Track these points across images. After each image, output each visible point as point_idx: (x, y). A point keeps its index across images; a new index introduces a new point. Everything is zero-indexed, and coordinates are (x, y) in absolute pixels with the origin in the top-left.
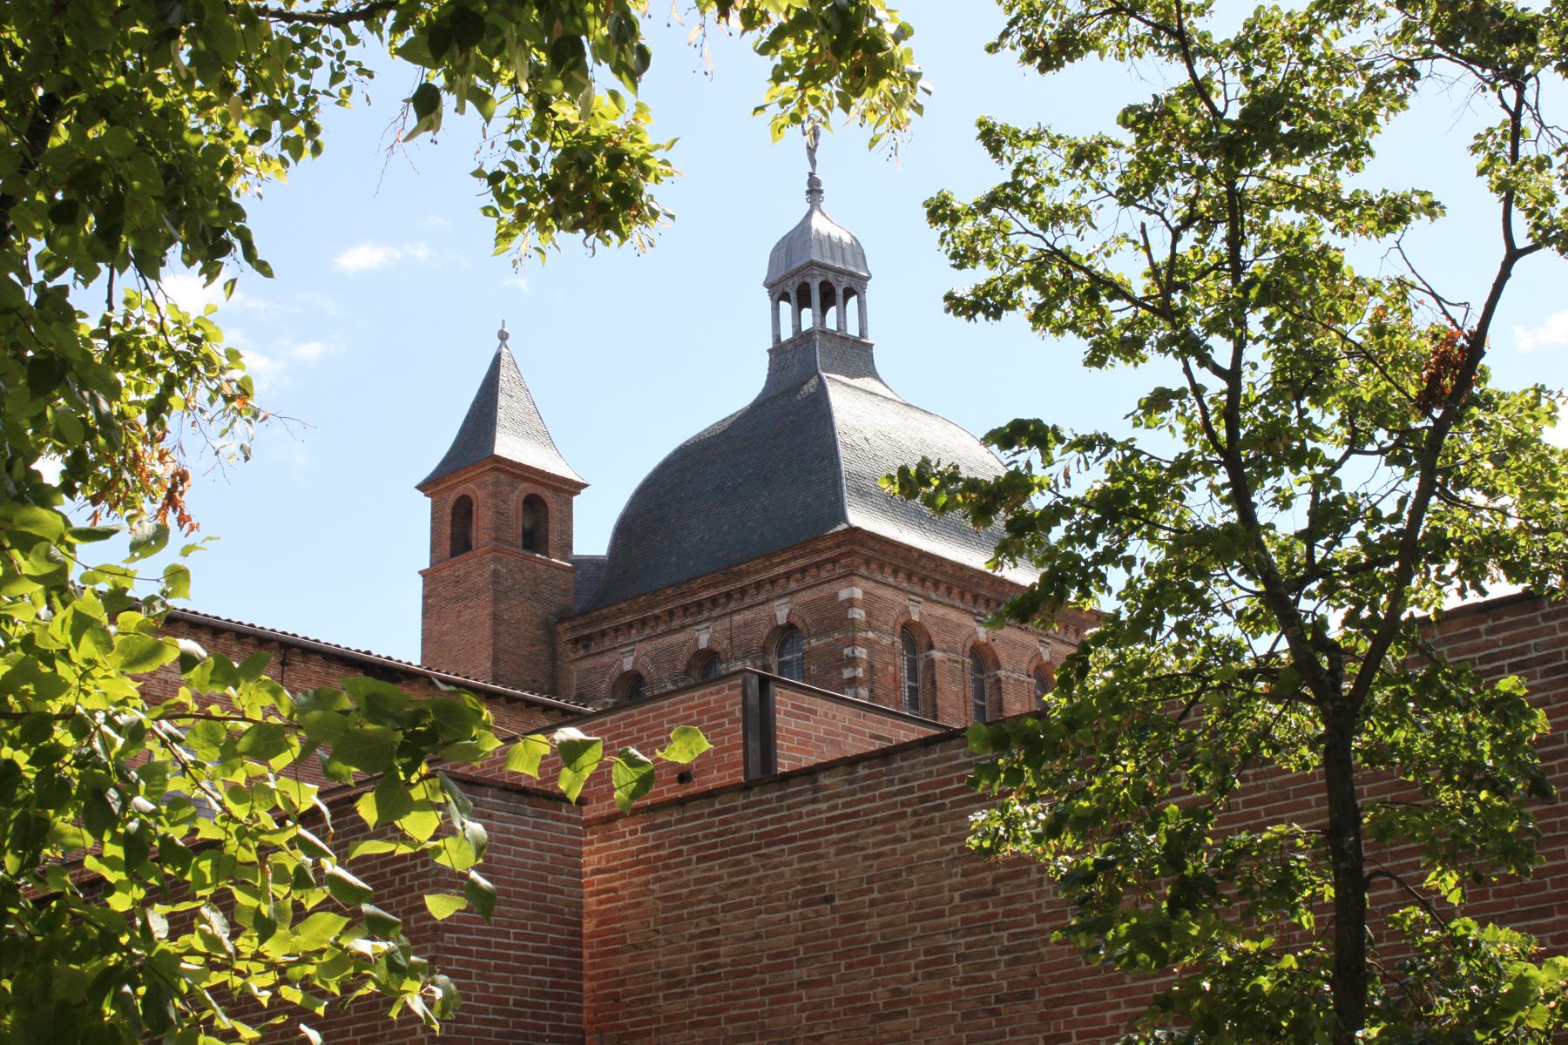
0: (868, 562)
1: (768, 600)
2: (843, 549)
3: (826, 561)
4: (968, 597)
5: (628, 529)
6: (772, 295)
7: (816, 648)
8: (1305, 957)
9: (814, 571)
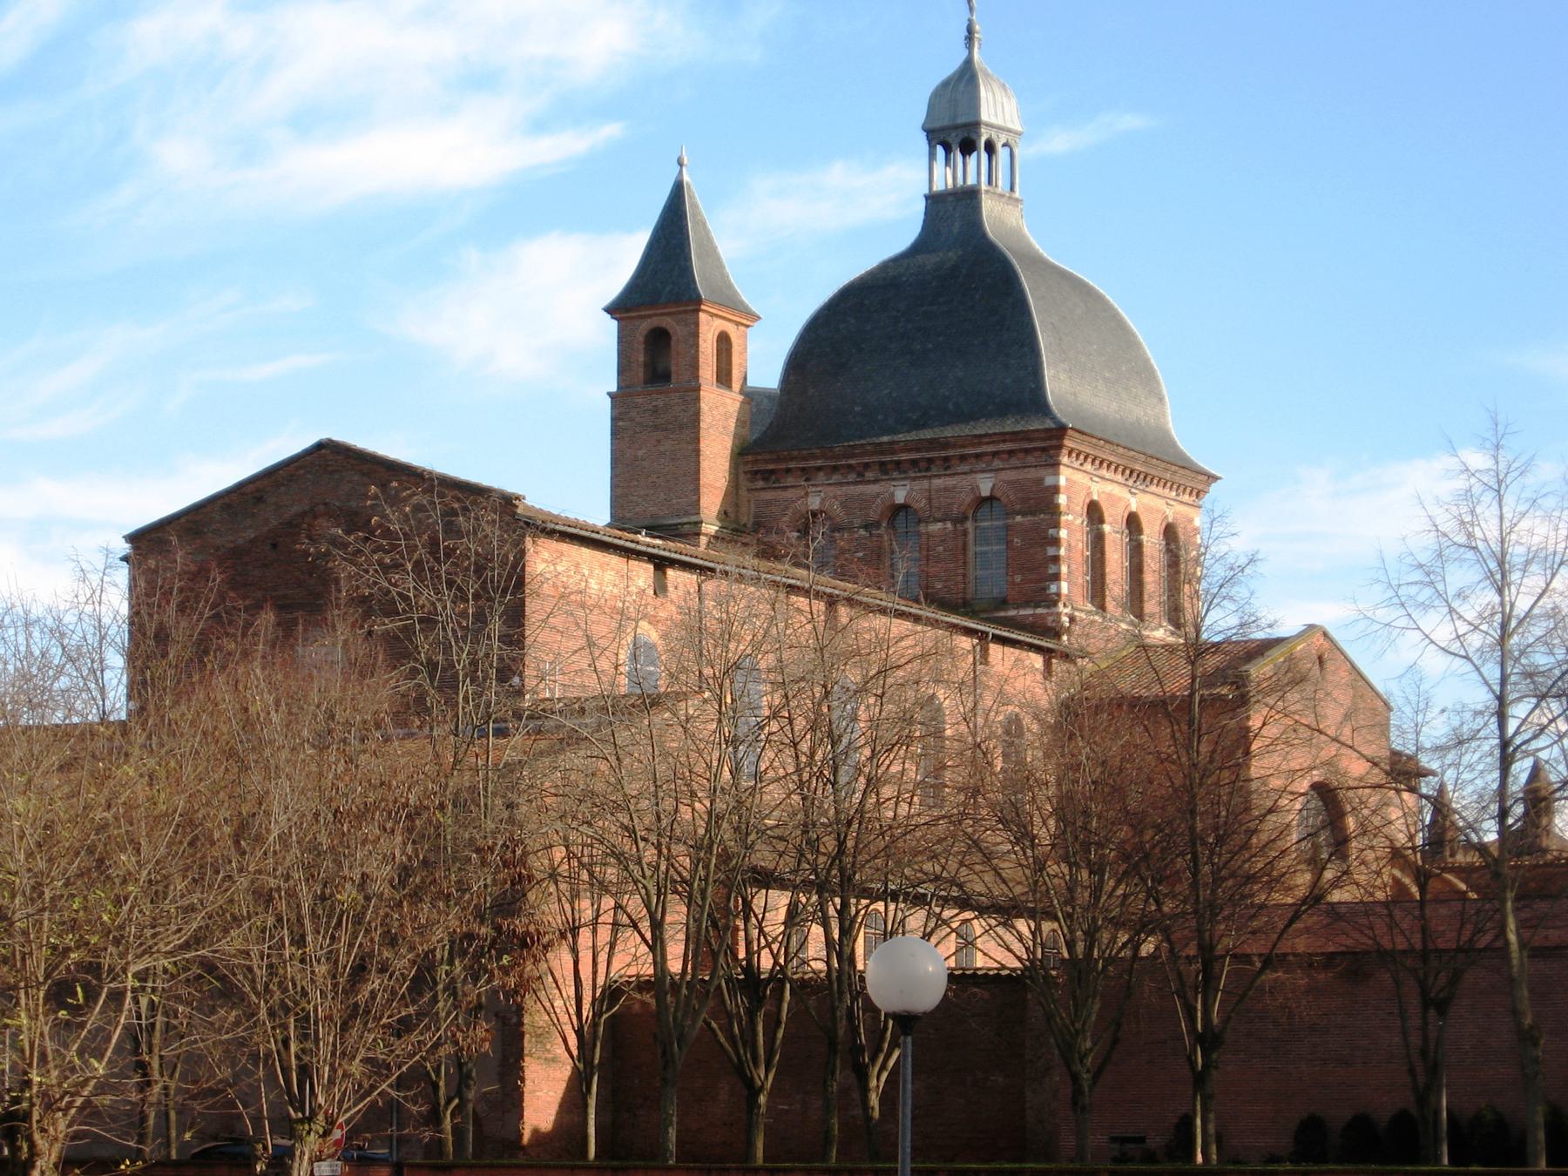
1: (972, 472)
3: (1035, 449)
5: (799, 362)
7: (1021, 524)
8: (445, 532)
9: (1021, 455)
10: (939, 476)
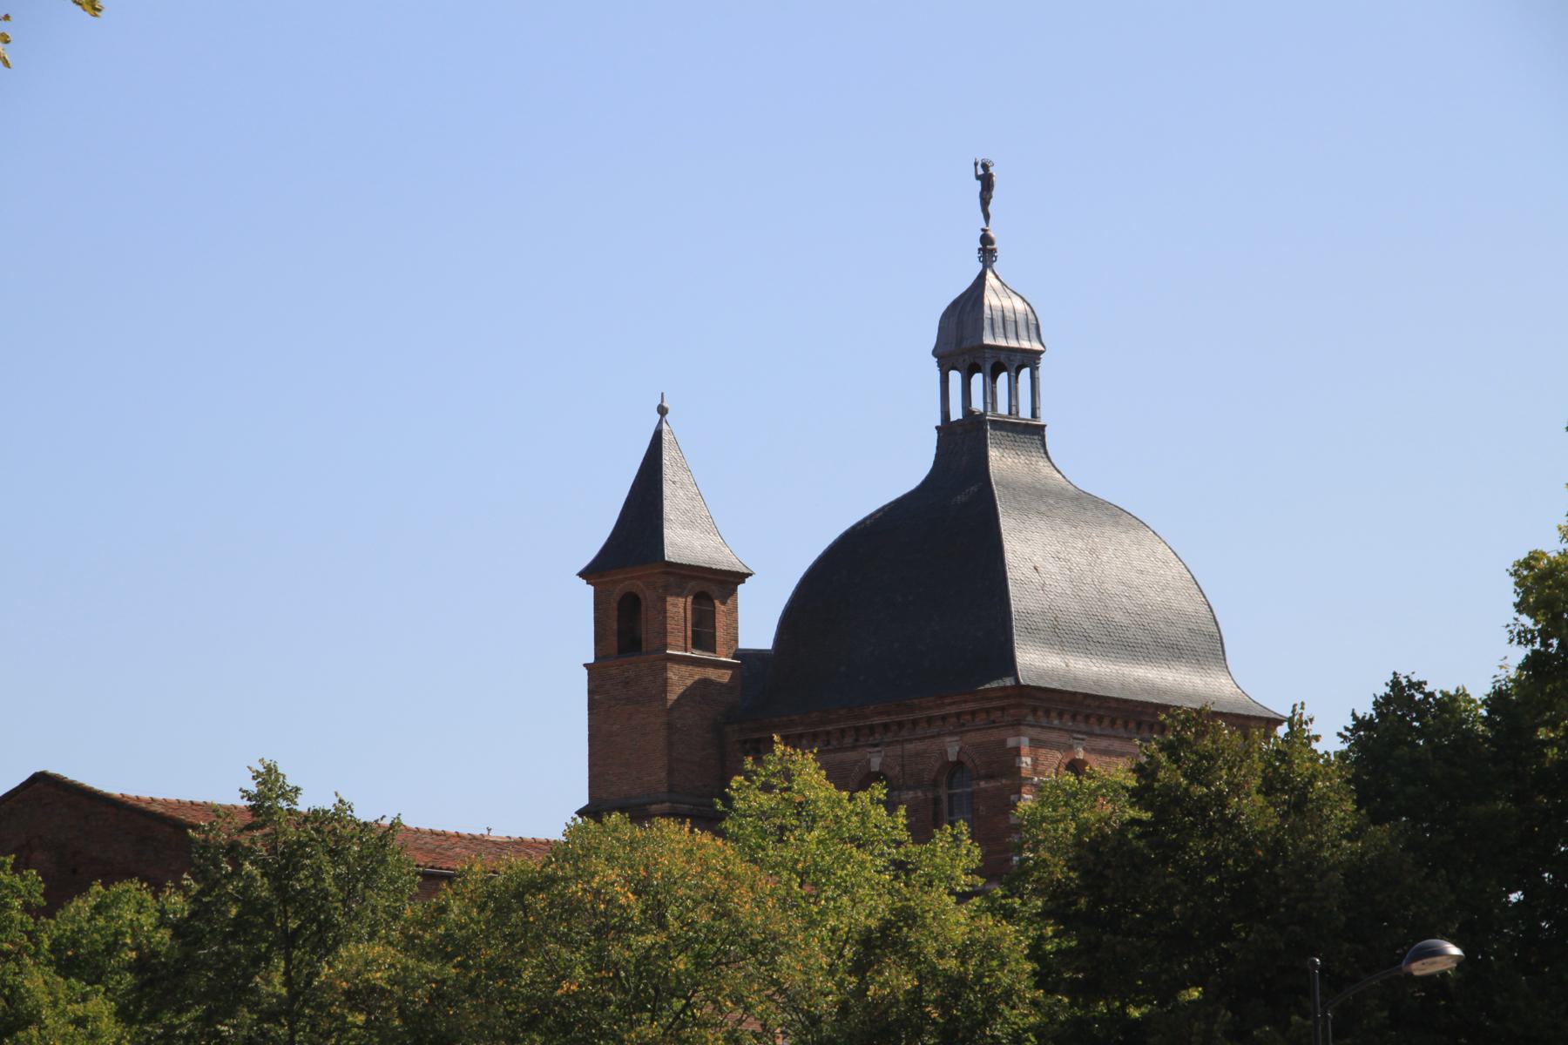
0: (1034, 711)
1: (939, 735)
2: (1012, 701)
4: (1132, 725)
6: (940, 365)
10: (910, 741)
